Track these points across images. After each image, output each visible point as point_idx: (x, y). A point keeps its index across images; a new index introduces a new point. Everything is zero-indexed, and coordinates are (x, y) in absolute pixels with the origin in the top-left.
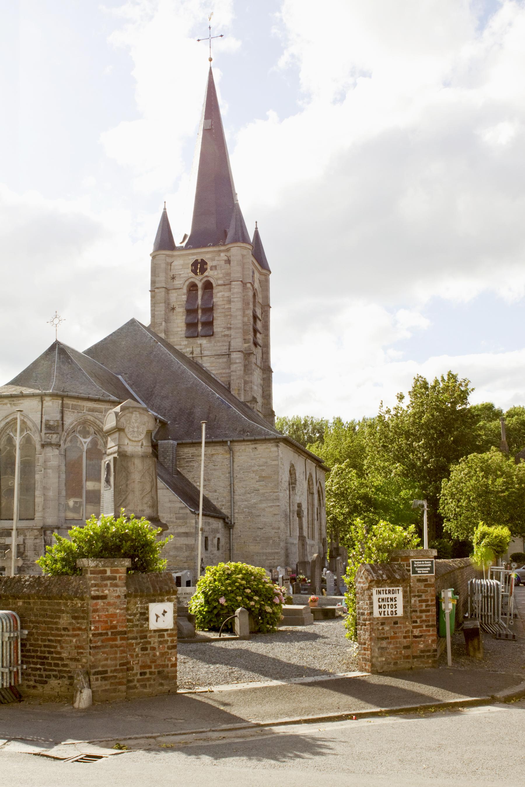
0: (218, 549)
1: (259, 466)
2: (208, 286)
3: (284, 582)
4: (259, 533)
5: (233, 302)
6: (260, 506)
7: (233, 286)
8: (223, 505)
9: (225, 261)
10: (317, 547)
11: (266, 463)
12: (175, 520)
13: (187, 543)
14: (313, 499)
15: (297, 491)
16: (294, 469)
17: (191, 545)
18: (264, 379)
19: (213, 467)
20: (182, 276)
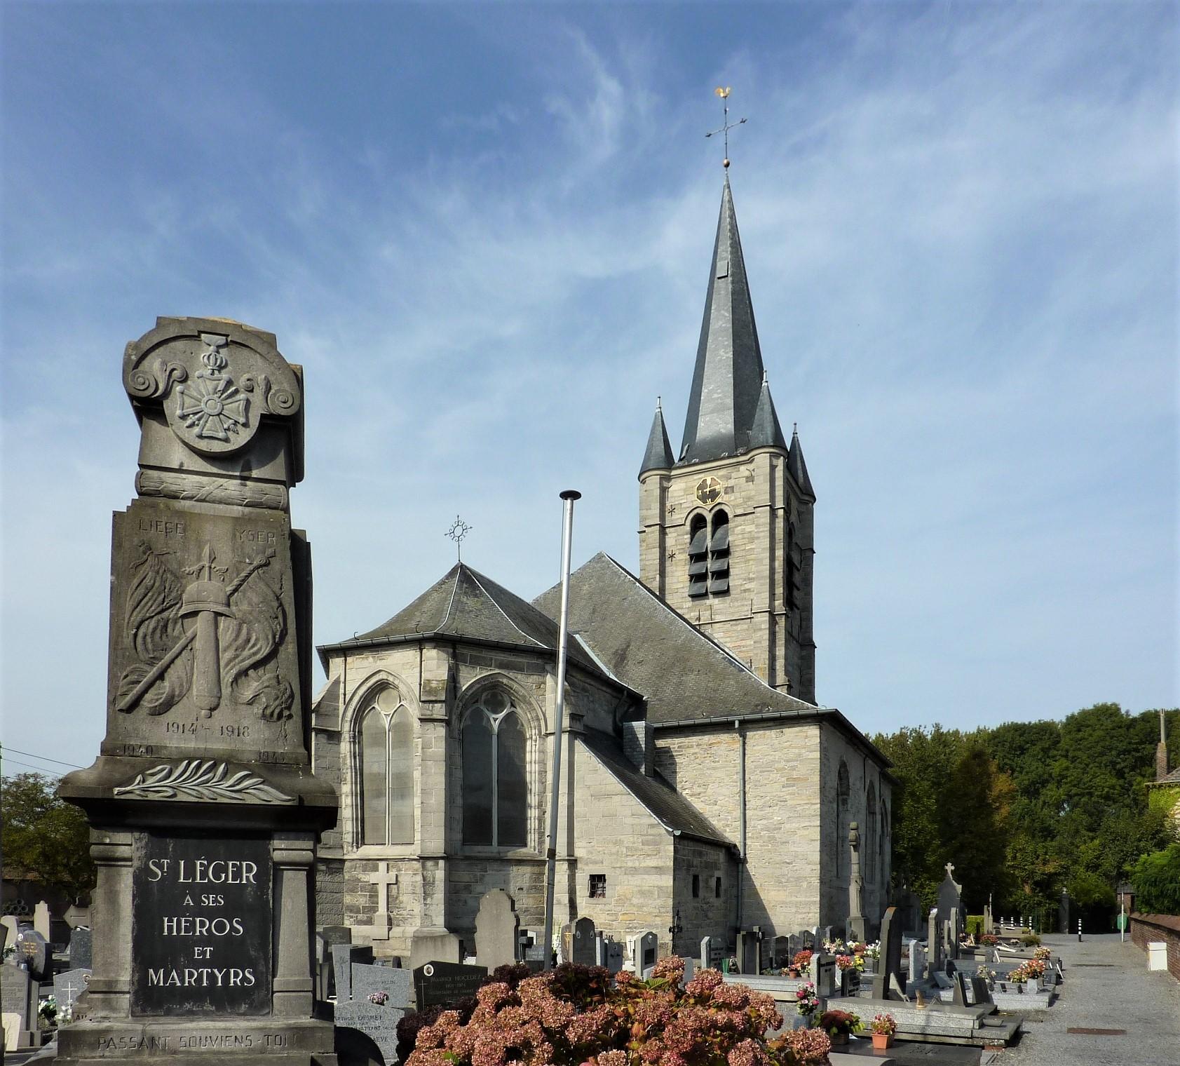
0: (718, 895)
2: (721, 518)
3: (822, 969)
4: (785, 870)
6: (788, 826)
11: (800, 755)
14: (874, 822)
16: (847, 771)
18: (802, 658)
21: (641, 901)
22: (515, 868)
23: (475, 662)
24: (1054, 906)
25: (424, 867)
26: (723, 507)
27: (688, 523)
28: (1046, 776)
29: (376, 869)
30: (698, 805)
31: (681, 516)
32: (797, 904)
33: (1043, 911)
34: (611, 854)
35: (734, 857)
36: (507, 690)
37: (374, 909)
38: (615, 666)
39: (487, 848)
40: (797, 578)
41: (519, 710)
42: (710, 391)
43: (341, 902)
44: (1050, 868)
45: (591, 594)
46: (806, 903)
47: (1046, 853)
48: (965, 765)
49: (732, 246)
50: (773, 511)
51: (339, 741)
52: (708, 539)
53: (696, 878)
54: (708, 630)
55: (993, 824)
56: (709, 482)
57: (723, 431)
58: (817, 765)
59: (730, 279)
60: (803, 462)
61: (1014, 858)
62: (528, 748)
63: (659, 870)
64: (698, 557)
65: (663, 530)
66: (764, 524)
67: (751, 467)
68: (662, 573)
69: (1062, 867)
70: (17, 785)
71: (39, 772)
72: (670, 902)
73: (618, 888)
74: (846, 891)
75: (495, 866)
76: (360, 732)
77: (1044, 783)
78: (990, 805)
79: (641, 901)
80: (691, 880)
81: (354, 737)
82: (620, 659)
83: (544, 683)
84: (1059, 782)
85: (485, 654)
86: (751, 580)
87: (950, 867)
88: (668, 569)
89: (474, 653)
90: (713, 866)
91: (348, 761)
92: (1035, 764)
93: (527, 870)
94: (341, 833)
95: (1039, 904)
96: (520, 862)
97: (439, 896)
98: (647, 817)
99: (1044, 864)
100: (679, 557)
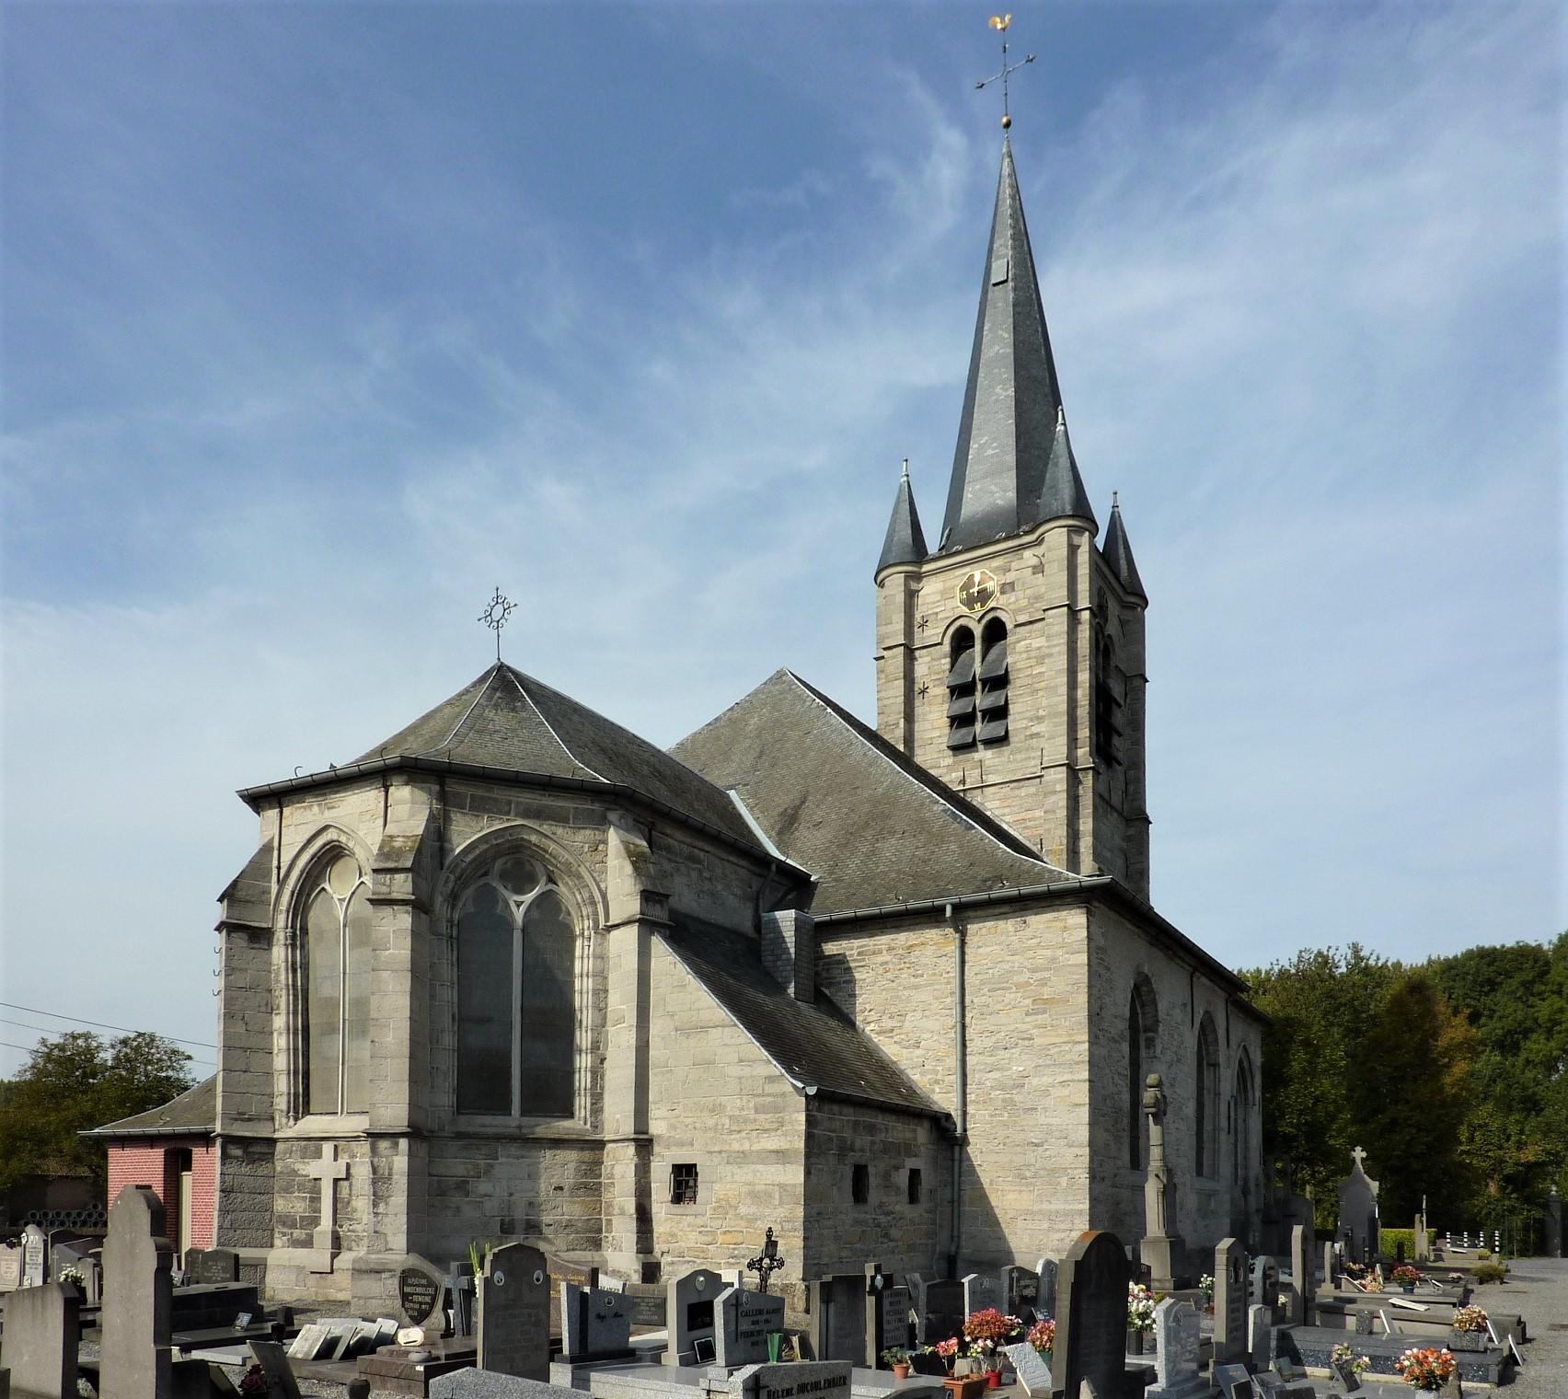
0: (913, 1198)
1: (1034, 971)
2: (996, 632)
4: (1031, 1157)
6: (1035, 1081)
8: (937, 1082)
9: (1034, 567)
10: (1227, 1197)
11: (1054, 959)
13: (783, 1180)
15: (1159, 1050)
18: (1128, 839)
21: (753, 1209)
22: (548, 1153)
23: (478, 807)
24: (1537, 1214)
25: (374, 1151)
26: (999, 614)
28: (1529, 1023)
30: (890, 1049)
31: (935, 632)
32: (1051, 1217)
33: (1517, 1221)
34: (706, 1130)
35: (946, 1135)
36: (539, 854)
37: (315, 1221)
38: (780, 833)
39: (499, 1120)
40: (1119, 719)
41: (562, 889)
42: (981, 447)
43: (269, 1209)
44: (1529, 1155)
45: (760, 732)
47: (1522, 1132)
48: (1398, 1002)
49: (1013, 238)
50: (1073, 613)
51: (270, 945)
52: (976, 663)
53: (860, 1173)
54: (976, 799)
55: (1441, 1090)
56: (977, 579)
57: (1000, 502)
58: (1082, 976)
59: (1011, 284)
60: (1127, 547)
61: (1471, 1140)
62: (578, 953)
63: (781, 1156)
64: (961, 690)
65: (910, 653)
66: (1058, 634)
68: (909, 717)
69: (1548, 1153)
70: (62, 1048)
71: (94, 1031)
72: (800, 1212)
73: (717, 1186)
74: (1140, 1189)
75: (514, 1149)
76: (304, 930)
77: (1526, 1033)
78: (1435, 1061)
79: (753, 1209)
80: (849, 1173)
81: (294, 937)
82: (787, 824)
83: (605, 842)
84: (1550, 1031)
85: (499, 793)
86: (1040, 719)
87: (1359, 1154)
88: (918, 711)
89: (479, 792)
90: (908, 1149)
91: (283, 977)
92: (1512, 1006)
93: (571, 1157)
94: (271, 1096)
95: (1512, 1211)
96: (558, 1143)
97: (399, 1199)
98: (764, 1064)
99: (1519, 1149)
100: (933, 691)
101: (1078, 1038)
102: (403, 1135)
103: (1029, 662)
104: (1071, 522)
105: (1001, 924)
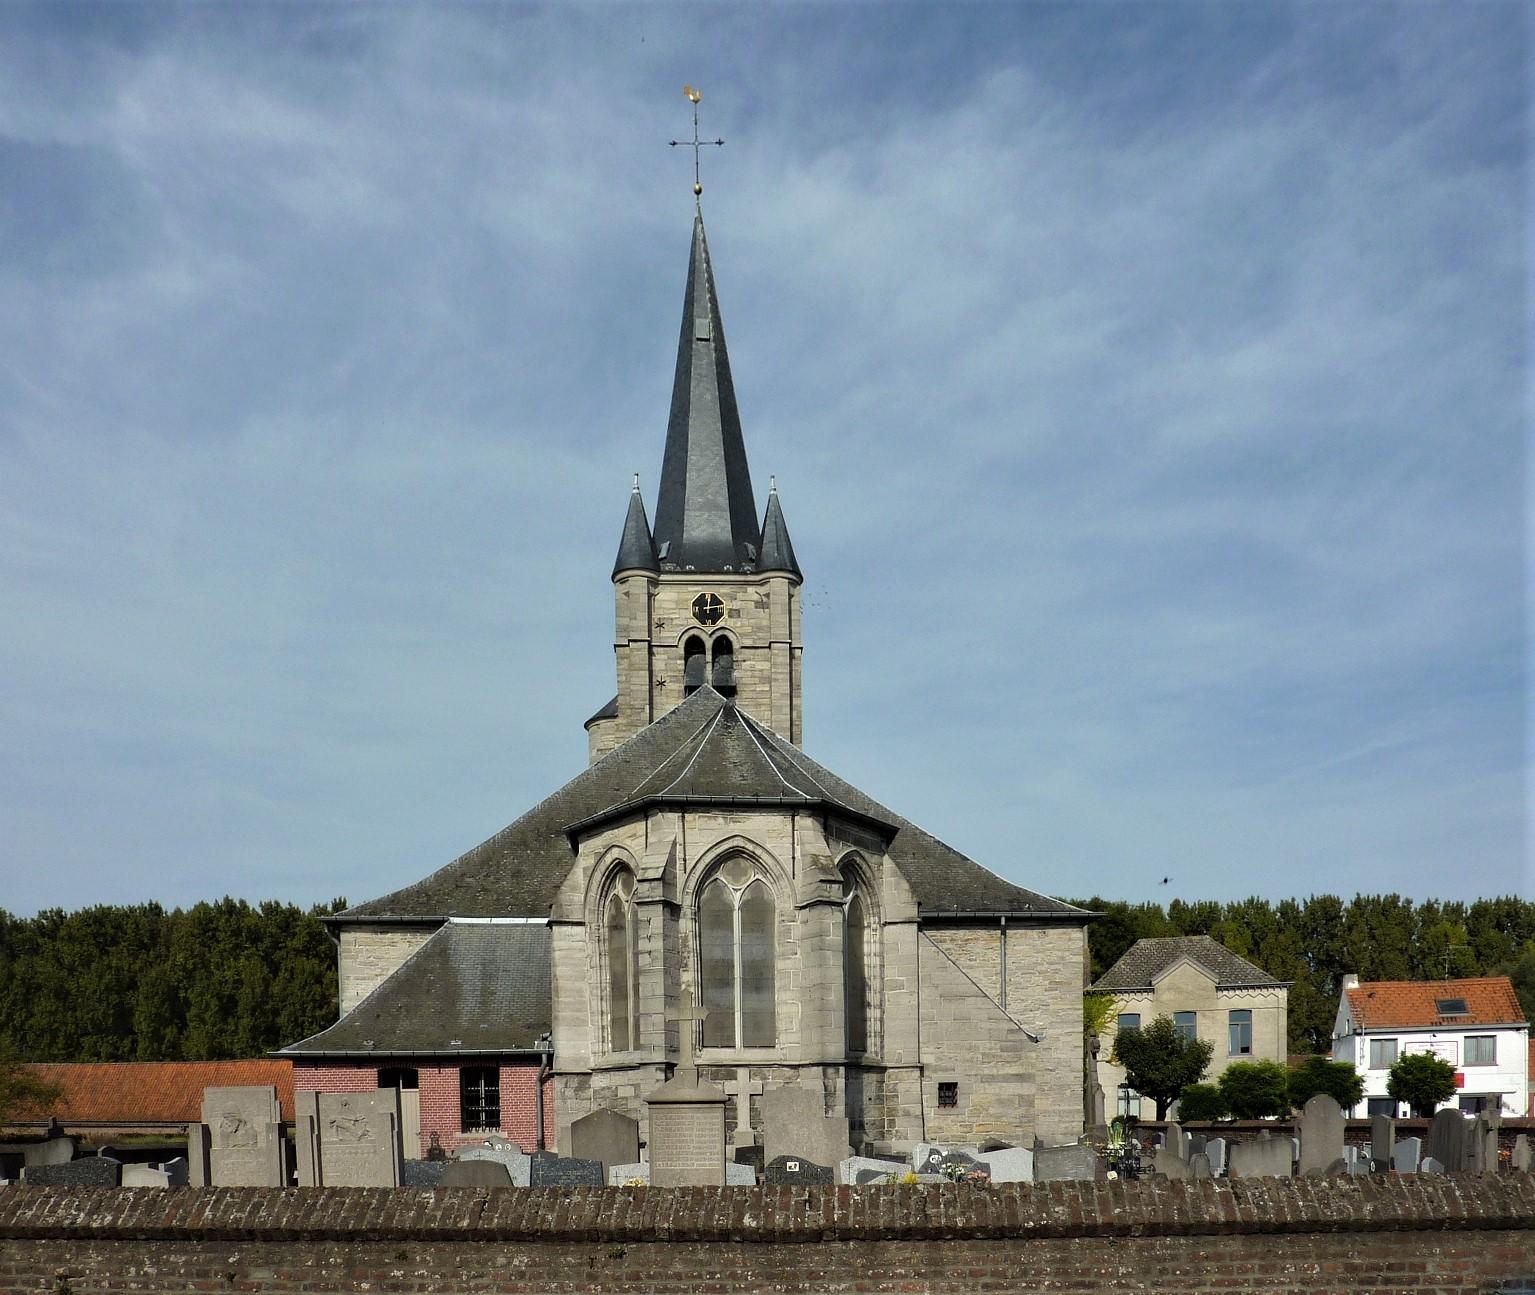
1: (1051, 964)
2: (723, 646)
5: (776, 680)
7: (776, 652)
9: (756, 602)
11: (1063, 958)
12: (999, 1052)
17: (1028, 1095)
19: (968, 962)
20: (675, 622)
25: (825, 1074)
26: (727, 633)
27: (682, 645)
29: (733, 1077)
31: (673, 634)
32: (1060, 1113)
34: (965, 1061)
46: (1070, 1112)
67: (763, 590)
88: (656, 700)
100: (670, 686)
101: (1077, 1007)
102: (841, 1065)
103: (752, 681)
104: (790, 576)
105: (1029, 932)
